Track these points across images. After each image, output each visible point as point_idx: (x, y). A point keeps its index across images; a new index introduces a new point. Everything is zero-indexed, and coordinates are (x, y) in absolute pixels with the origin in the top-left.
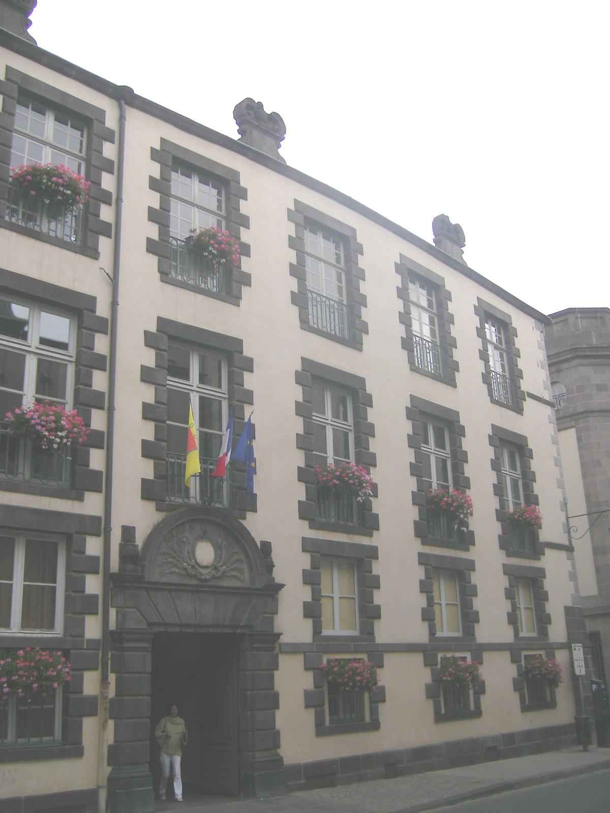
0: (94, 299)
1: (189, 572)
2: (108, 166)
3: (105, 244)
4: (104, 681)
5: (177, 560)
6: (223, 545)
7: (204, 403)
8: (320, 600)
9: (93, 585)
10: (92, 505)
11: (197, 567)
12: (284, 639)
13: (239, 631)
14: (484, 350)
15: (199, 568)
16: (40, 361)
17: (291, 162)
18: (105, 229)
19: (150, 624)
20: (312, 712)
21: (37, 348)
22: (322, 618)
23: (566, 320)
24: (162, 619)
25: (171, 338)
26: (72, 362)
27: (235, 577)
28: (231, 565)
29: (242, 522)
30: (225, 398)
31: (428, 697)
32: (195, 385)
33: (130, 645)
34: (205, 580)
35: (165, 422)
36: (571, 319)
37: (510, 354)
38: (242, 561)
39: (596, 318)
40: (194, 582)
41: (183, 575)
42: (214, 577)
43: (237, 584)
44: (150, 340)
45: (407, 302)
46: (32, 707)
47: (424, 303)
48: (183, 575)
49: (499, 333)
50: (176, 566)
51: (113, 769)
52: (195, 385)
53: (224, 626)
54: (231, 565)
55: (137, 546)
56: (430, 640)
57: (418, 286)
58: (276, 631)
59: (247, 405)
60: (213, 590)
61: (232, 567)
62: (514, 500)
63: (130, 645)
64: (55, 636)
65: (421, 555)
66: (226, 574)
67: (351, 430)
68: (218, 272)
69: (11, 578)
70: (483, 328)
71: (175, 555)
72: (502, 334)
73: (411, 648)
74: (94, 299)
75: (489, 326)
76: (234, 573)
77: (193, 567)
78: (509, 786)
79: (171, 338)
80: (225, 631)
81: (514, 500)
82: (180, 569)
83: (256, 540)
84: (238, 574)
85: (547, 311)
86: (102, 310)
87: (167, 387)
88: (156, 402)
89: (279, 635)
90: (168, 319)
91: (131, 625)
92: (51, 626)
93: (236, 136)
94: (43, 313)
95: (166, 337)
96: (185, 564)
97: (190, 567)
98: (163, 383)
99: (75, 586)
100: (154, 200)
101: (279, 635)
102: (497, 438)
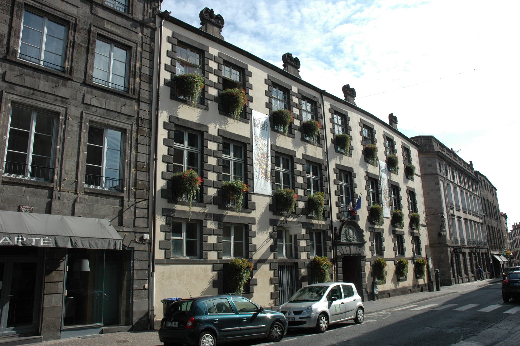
14: (269, 102)
17: (400, 130)
20: (372, 278)
23: (418, 140)
25: (307, 161)
30: (199, 152)
31: (372, 276)
35: (222, 173)
36: (419, 139)
37: (393, 150)
39: (428, 139)
45: (334, 124)
47: (340, 122)
49: (390, 143)
56: (395, 257)
57: (278, 89)
62: (347, 197)
70: (333, 118)
72: (286, 94)
75: (306, 103)
78: (426, 299)
79: (307, 161)
81: (347, 197)
85: (409, 136)
87: (174, 147)
93: (282, 68)
95: (338, 170)
98: (172, 146)
100: (266, 99)
101: (365, 257)
102: (305, 160)
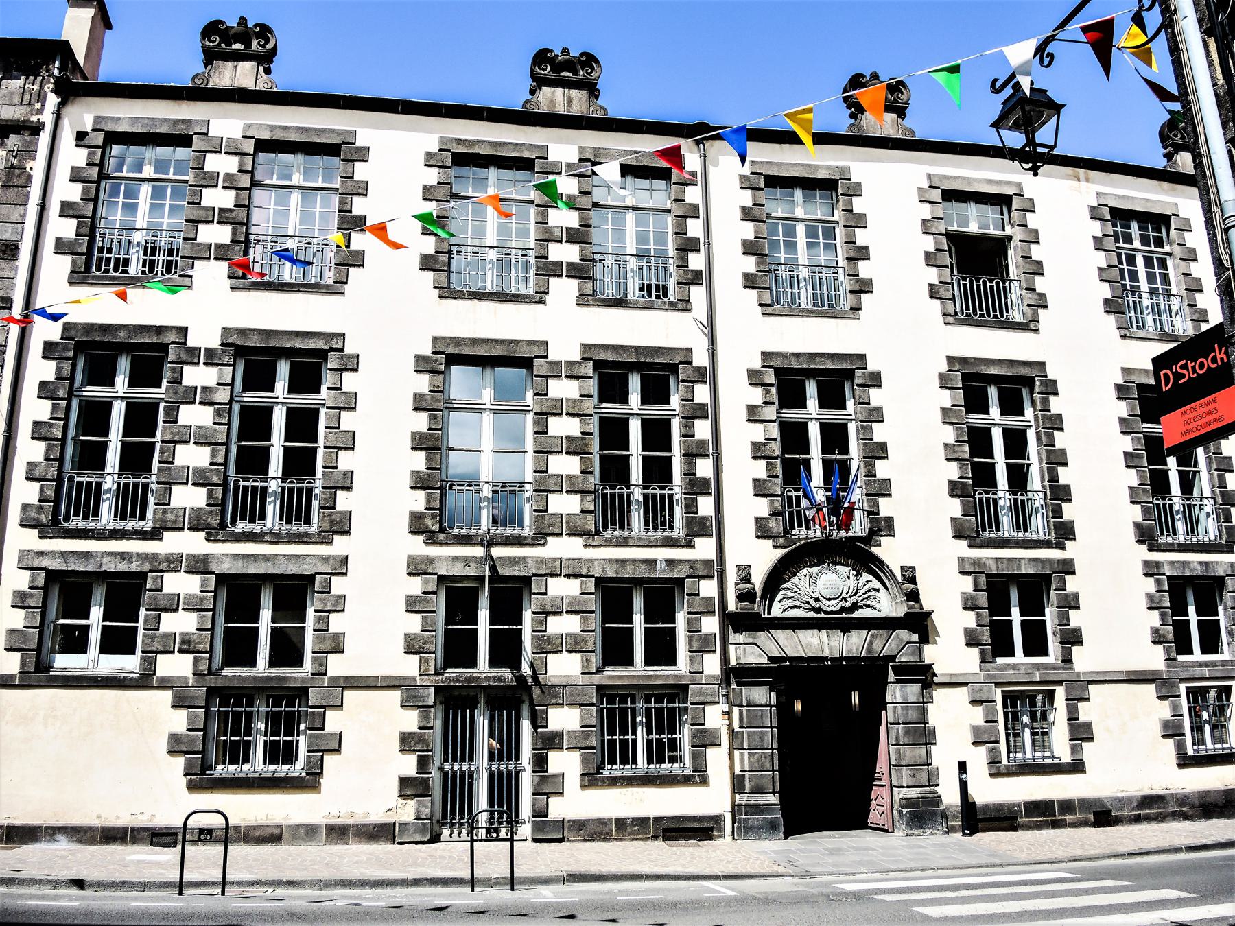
2: (693, 212)
3: (697, 294)
7: (1008, 433)
9: (711, 625)
10: (705, 548)
16: (643, 420)
18: (695, 278)
19: (771, 659)
21: (639, 409)
24: (785, 653)
26: (851, 420)
28: (864, 594)
29: (874, 549)
38: (878, 591)
42: (843, 610)
43: (875, 614)
44: (755, 378)
46: (1027, 732)
64: (303, 674)
65: (1147, 564)
67: (1030, 426)
68: (632, 277)
73: (390, 684)
84: (873, 603)
86: (701, 359)
88: (583, 433)
99: (694, 629)
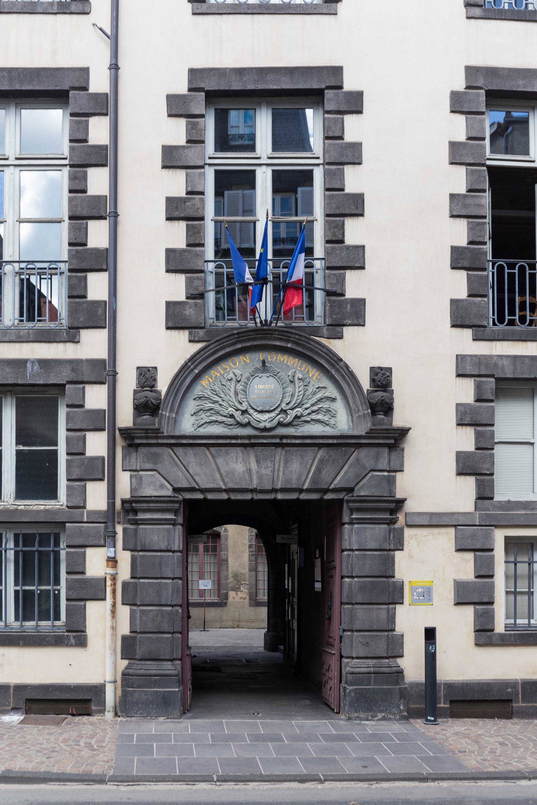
0: (85, 71)
1: (238, 419)
4: (113, 561)
5: (221, 405)
6: (296, 379)
8: (493, 449)
11: (251, 411)
12: (411, 506)
13: (329, 496)
15: (255, 413)
22: (495, 476)
27: (318, 421)
28: (312, 405)
32: (264, 156)
33: (148, 516)
34: (265, 429)
40: (248, 431)
41: (231, 425)
42: (280, 424)
43: (328, 431)
48: (231, 425)
50: (218, 413)
51: (129, 663)
52: (264, 156)
53: (301, 491)
54: (312, 405)
55: (159, 393)
58: (399, 495)
59: (350, 167)
60: (278, 441)
61: (315, 408)
63: (148, 516)
66: (303, 419)
69: (56, 445)
71: (217, 398)
74: (85, 71)
76: (314, 416)
77: (244, 412)
80: (304, 496)
82: (225, 416)
83: (354, 367)
89: (402, 501)
90: (502, 91)
91: (149, 491)
92: (53, 494)
94: (23, 111)
96: (230, 409)
97: (239, 413)
101: (402, 501)
